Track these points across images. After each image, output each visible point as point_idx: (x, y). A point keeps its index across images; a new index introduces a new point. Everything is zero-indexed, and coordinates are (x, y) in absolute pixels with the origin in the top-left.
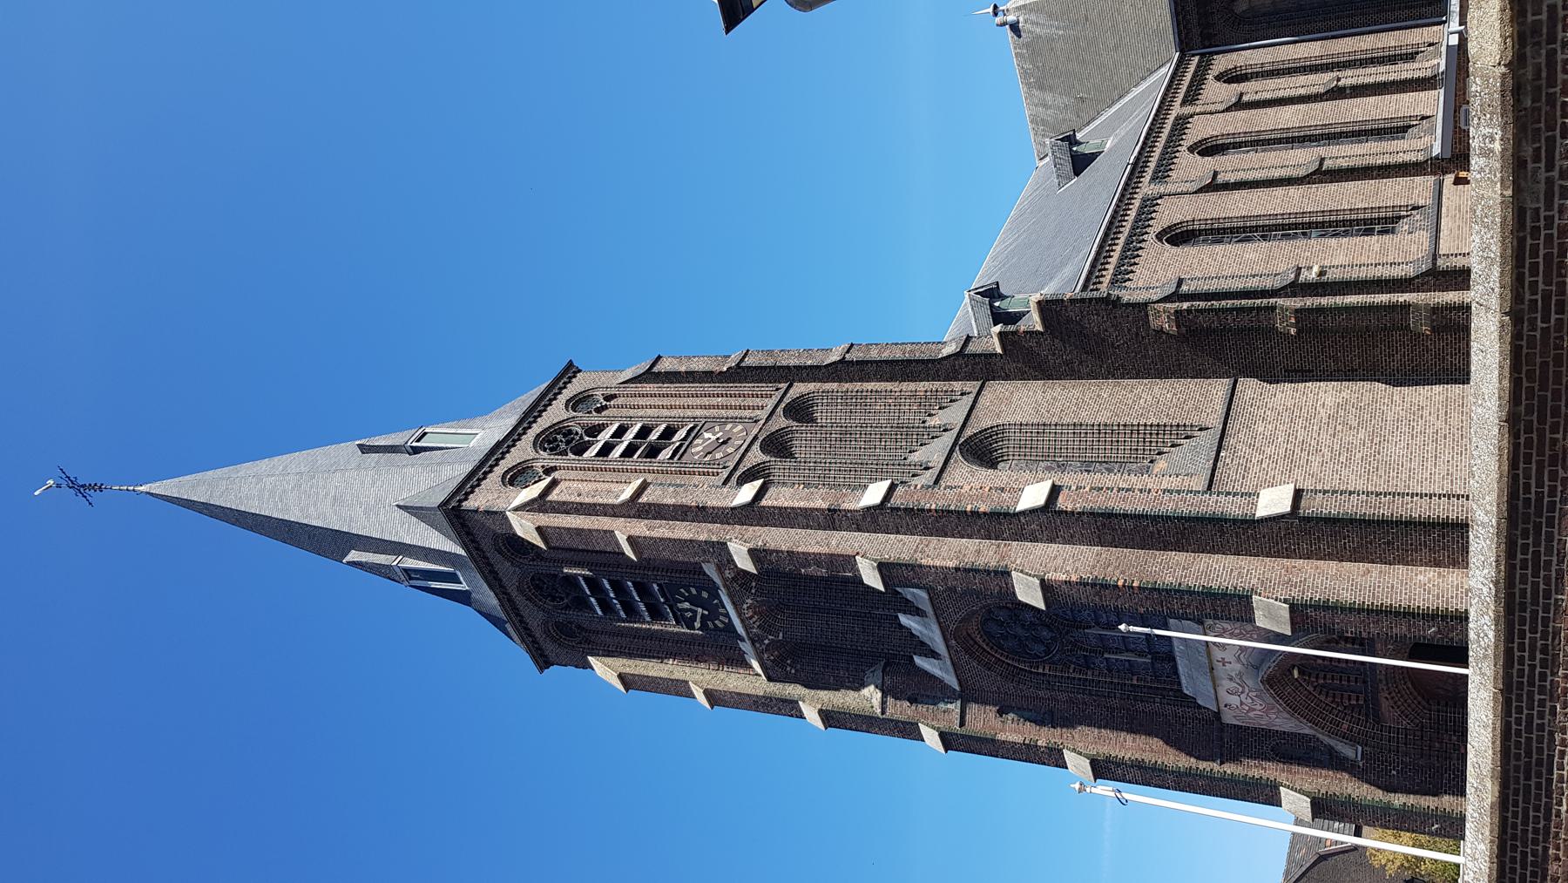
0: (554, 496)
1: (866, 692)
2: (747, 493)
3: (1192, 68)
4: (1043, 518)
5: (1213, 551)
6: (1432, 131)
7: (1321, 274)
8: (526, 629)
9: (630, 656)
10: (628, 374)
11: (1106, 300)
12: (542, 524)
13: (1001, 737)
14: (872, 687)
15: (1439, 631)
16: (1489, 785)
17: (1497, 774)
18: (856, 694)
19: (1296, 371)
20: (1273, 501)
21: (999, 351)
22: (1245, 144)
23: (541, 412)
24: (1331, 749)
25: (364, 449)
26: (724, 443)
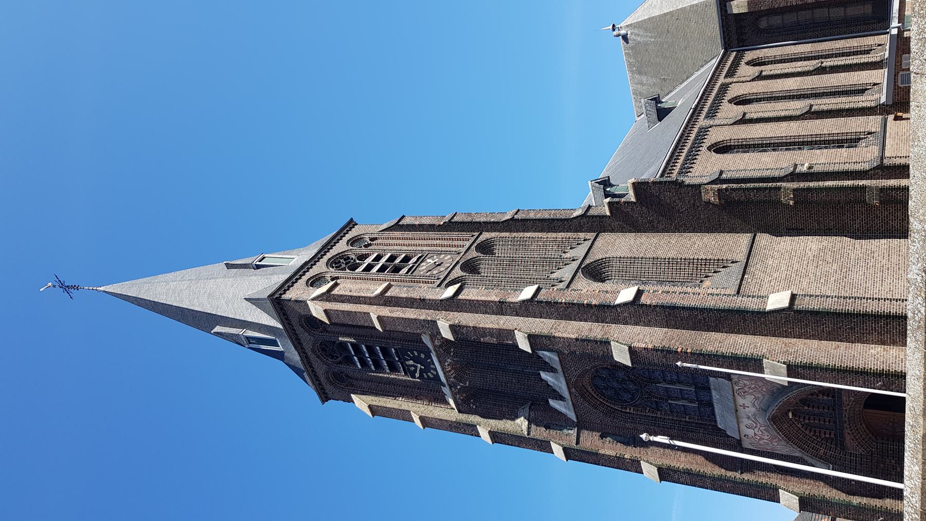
0: (336, 292)
1: (518, 421)
3: (732, 58)
5: (738, 332)
6: (880, 91)
7: (810, 168)
8: (315, 375)
9: (376, 394)
10: (385, 226)
11: (675, 183)
12: (328, 308)
13: (602, 452)
14: (522, 418)
18: (512, 423)
19: (793, 229)
20: (778, 300)
21: (608, 214)
25: (229, 266)
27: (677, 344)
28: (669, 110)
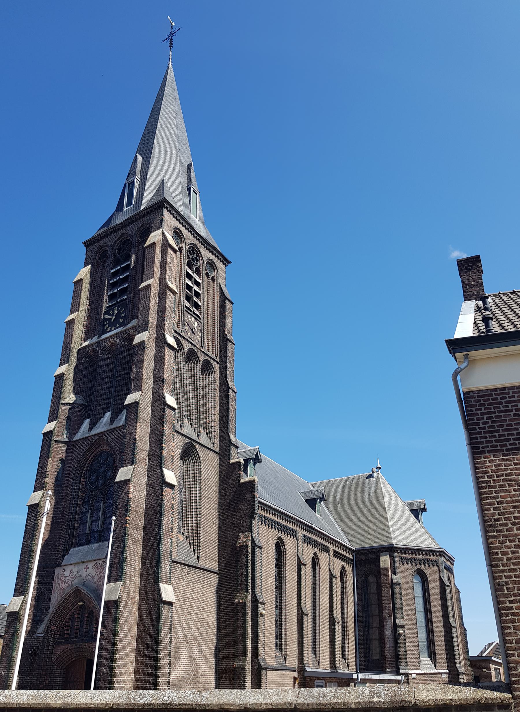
0: (169, 251)
1: (73, 396)
2: (171, 341)
3: (348, 555)
4: (159, 481)
5: (143, 563)
6: (314, 667)
7: (261, 615)
8: (105, 237)
9: (91, 285)
10: (224, 288)
11: (254, 513)
12: (157, 245)
14: (75, 399)
15: (104, 674)
16: (60, 702)
17: (65, 706)
20: (167, 592)
21: (231, 461)
22: (315, 579)
23: (206, 247)
24: (42, 621)
25: (189, 166)
26: (193, 331)
27: (133, 516)
28: (313, 507)
